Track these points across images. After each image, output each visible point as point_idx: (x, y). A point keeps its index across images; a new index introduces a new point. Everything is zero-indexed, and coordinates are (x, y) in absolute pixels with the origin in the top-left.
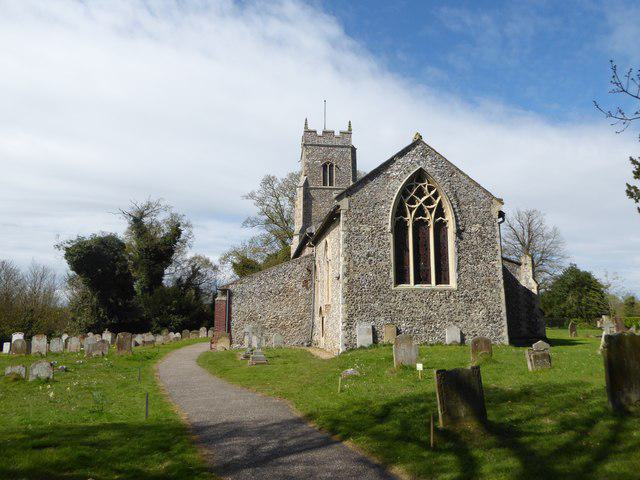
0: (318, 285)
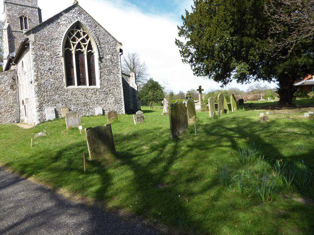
0: (20, 88)
